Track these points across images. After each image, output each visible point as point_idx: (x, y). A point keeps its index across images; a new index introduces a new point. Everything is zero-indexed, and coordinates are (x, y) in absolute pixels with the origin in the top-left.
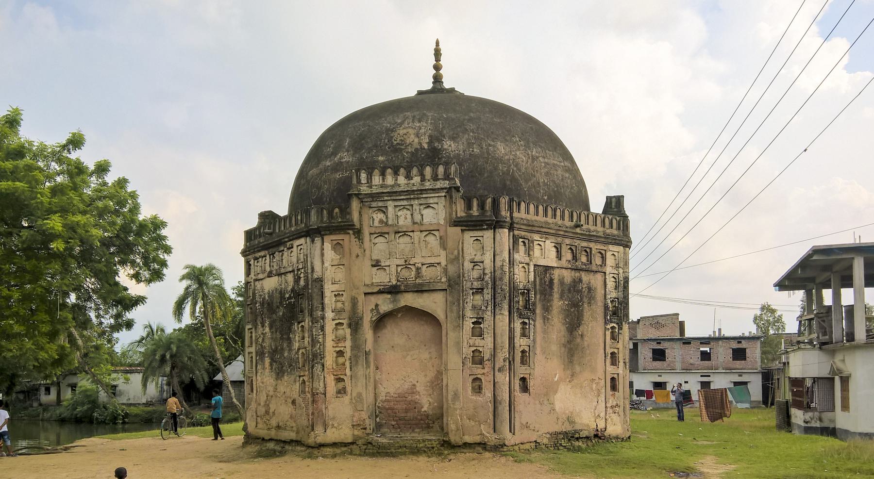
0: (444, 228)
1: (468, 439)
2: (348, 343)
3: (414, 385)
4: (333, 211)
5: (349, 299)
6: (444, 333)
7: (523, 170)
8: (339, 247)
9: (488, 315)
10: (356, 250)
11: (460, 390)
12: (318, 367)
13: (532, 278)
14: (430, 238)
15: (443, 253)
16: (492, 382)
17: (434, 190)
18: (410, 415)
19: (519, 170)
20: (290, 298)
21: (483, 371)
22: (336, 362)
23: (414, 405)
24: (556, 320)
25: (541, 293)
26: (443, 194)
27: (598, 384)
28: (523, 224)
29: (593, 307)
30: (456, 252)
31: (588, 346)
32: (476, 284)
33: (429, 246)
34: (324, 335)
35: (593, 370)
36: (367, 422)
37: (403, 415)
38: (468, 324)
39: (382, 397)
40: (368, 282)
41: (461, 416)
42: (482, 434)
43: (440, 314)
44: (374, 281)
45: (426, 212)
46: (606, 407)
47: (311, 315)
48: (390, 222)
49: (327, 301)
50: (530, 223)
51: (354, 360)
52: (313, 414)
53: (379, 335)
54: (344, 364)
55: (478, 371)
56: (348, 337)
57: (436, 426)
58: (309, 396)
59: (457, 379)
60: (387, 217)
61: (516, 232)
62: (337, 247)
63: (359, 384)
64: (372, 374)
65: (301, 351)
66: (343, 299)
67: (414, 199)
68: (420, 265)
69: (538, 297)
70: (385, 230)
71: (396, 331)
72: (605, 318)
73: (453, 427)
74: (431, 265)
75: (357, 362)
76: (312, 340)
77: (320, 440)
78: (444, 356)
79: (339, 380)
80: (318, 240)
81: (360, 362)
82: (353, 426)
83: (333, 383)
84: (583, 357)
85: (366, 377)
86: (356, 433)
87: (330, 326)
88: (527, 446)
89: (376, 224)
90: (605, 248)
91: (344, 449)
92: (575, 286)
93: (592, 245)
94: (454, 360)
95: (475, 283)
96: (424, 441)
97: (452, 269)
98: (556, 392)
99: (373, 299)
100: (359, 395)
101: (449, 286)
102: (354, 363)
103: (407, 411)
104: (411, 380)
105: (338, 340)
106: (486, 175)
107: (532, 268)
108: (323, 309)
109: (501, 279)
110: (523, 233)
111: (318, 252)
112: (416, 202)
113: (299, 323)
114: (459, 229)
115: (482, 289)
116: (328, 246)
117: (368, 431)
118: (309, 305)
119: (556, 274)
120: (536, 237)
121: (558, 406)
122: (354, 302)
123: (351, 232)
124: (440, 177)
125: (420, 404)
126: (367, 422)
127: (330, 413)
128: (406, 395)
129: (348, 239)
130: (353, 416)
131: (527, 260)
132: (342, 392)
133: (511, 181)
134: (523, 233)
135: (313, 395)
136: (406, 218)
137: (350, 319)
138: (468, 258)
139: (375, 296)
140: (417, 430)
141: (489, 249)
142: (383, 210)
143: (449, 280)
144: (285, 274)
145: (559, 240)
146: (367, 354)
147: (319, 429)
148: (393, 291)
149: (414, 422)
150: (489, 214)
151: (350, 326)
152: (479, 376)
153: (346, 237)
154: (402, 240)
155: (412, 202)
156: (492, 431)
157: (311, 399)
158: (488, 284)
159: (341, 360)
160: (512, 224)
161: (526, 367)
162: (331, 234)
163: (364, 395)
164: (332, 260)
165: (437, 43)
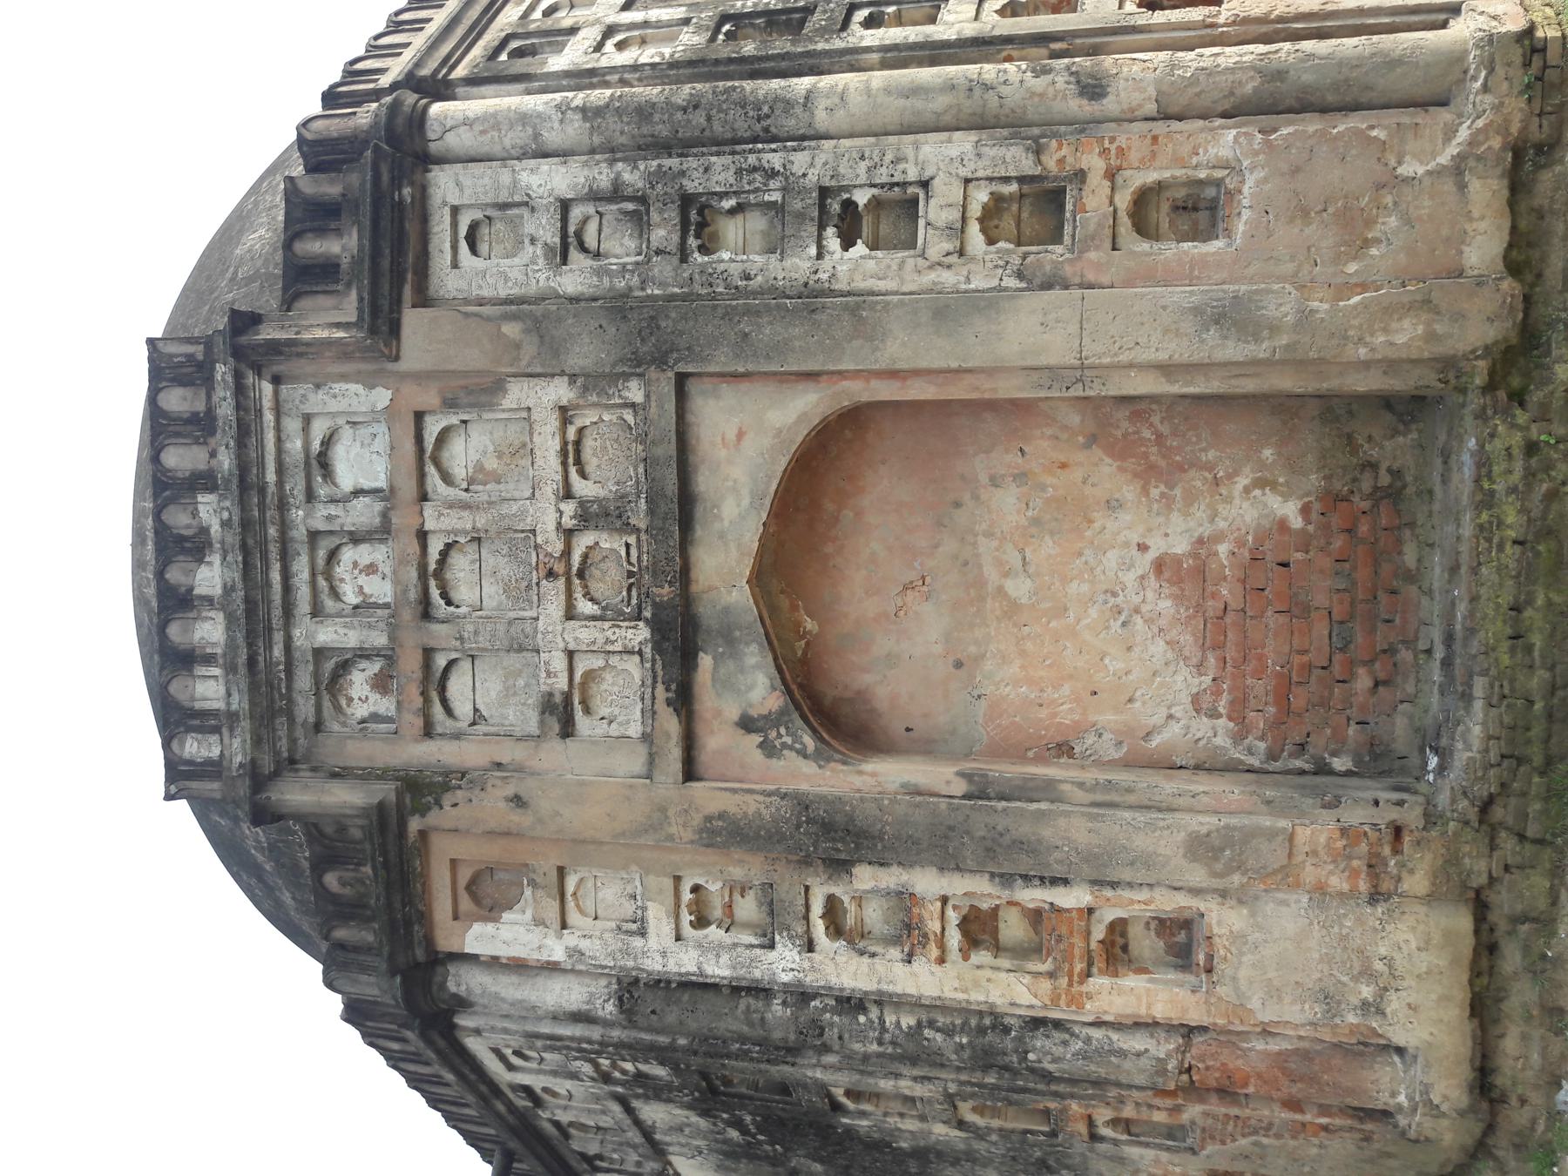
0: (409, 389)
1: (1483, 247)
2: (927, 883)
3: (1159, 566)
4: (334, 898)
5: (712, 856)
6: (885, 391)
8: (487, 888)
9: (810, 166)
10: (491, 805)
11: (1180, 295)
12: (1043, 1049)
14: (461, 456)
15: (517, 394)
16: (1160, 127)
17: (245, 431)
18: (1321, 592)
20: (738, 1124)
21: (1096, 180)
22: (1023, 952)
23: (1268, 561)
26: (267, 388)
30: (511, 330)
32: (663, 233)
33: (492, 464)
34: (882, 1000)
36: (1356, 816)
37: (1321, 629)
38: (852, 265)
39: (1217, 733)
40: (637, 763)
41: (1345, 289)
42: (1458, 169)
43: (794, 412)
44: (635, 730)
45: (346, 477)
47: (791, 1051)
48: (380, 640)
49: (719, 969)
51: (1014, 860)
52: (1293, 1105)
53: (897, 727)
54: (1036, 917)
55: (1095, 203)
56: (891, 878)
57: (1393, 449)
58: (1193, 1112)
59: (1133, 317)
60: (363, 654)
62: (486, 895)
63: (1141, 842)
64: (1090, 776)
65: (971, 1117)
66: (714, 887)
67: (284, 526)
68: (569, 508)
70: (410, 663)
71: (884, 644)
73: (1406, 334)
74: (572, 455)
75: (1019, 845)
76: (914, 1061)
77: (1450, 1089)
78: (1008, 388)
79: (1116, 951)
80: (463, 981)
81: (1024, 830)
82: (1375, 897)
83: (1131, 981)
85: (1105, 803)
86: (1417, 882)
87: (841, 969)
89: (385, 705)
91: (1511, 959)
94: (1035, 334)
96: (1487, 501)
97: (586, 352)
99: (718, 739)
100: (1202, 848)
101: (660, 361)
102: (1025, 864)
103: (1296, 609)
104: (1130, 578)
105: (908, 933)
108: (761, 991)
109: (644, 112)
111: (509, 988)
112: (297, 515)
113: (836, 1107)
114: (412, 319)
115: (687, 201)
116: (479, 938)
117: (1412, 816)
118: (743, 1055)
122: (725, 834)
123: (414, 824)
124: (200, 406)
125: (1260, 539)
126: (1356, 816)
127: (1295, 1014)
128: (1213, 607)
129: (453, 840)
130: (1320, 889)
132: (1182, 943)
135: (1193, 1091)
136: (371, 569)
137: (806, 862)
138: (542, 278)
139: (700, 729)
140: (1410, 557)
141: (505, 177)
142: (334, 670)
143: (635, 365)
144: (647, 1133)
146: (980, 790)
147: (1389, 1086)
148: (678, 639)
149: (1363, 574)
150: (354, 179)
151: (839, 867)
152: (1123, 200)
153: (443, 850)
154: (464, 593)
155: (299, 533)
156: (1444, 115)
157: (1219, 1108)
158: (660, 174)
159: (1013, 928)
162: (425, 918)
163: (1205, 823)
164: (539, 922)
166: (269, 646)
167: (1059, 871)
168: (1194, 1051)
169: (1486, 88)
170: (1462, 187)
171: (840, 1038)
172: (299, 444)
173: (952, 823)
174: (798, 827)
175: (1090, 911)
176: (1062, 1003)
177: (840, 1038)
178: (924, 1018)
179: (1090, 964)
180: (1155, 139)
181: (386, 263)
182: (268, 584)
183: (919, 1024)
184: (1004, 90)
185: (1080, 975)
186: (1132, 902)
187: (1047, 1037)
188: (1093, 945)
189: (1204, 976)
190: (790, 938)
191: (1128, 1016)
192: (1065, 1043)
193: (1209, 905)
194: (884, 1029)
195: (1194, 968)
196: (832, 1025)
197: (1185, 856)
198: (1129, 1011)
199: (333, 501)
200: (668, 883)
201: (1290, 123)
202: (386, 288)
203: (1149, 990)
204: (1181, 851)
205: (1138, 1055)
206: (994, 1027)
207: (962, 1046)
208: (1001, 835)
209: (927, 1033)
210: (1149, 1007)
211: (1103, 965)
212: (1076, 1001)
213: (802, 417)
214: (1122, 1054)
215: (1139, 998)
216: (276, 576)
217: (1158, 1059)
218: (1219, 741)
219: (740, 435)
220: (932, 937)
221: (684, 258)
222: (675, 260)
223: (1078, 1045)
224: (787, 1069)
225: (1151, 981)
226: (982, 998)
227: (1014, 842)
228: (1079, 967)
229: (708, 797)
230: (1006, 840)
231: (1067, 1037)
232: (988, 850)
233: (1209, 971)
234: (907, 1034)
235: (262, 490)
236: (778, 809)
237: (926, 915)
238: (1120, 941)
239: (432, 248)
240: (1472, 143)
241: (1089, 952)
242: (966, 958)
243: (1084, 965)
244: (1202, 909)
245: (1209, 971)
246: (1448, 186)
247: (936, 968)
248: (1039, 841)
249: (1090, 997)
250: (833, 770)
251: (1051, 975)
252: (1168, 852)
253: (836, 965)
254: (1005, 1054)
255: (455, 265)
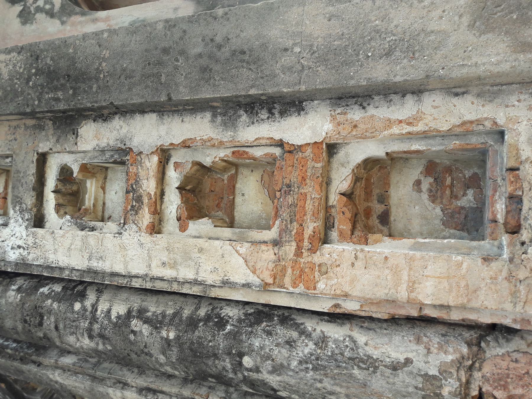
79: (368, 209)
102: (246, 85)
167: (284, 85)
168: (487, 369)
171: (57, 328)
173: (165, 44)
174: (28, 80)
175: (332, 149)
176: (287, 281)
177: (57, 328)
178: (136, 306)
179: (328, 225)
183: (129, 314)
185: (311, 239)
186: (389, 123)
187: (269, 333)
188: (334, 199)
189: (505, 239)
190: (22, 211)
191: (379, 303)
192: (290, 343)
193: (512, 112)
194: (94, 319)
195: (488, 229)
196: (50, 312)
197: (471, 26)
198: (381, 293)
203: (412, 259)
204: (466, 20)
205: (395, 367)
206: (208, 318)
207: (167, 341)
208: (219, 47)
209: (136, 324)
210: (411, 289)
211: (346, 227)
212: (305, 277)
214: (371, 364)
215: (396, 271)
217: (427, 377)
220: (146, 200)
223: (307, 348)
224: (33, 368)
225: (415, 247)
226: (190, 275)
227: (234, 53)
228: (311, 227)
230: (226, 52)
231: (295, 334)
232: (204, 70)
233: (514, 230)
234: (115, 325)
236: (15, 66)
237: (142, 173)
238: (379, 208)
241: (328, 208)
242: (183, 228)
243: (319, 224)
244: (501, 121)
245: (514, 230)
247: (146, 238)
248: (264, 46)
249: (323, 270)
250: (73, 24)
251: (276, 243)
252: (444, 25)
253: (54, 239)
254: (216, 356)
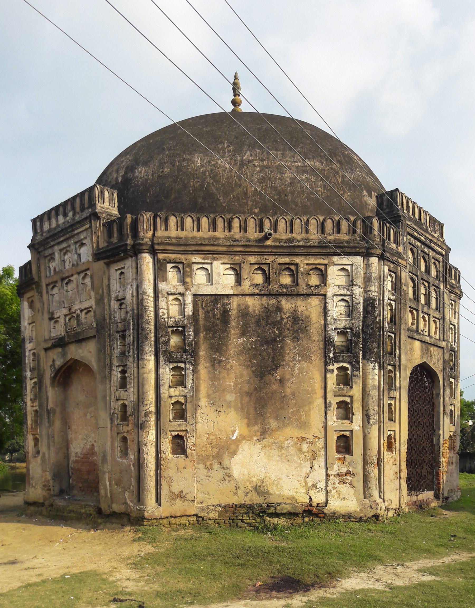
7: (223, 180)
13: (189, 310)
16: (136, 442)
19: (218, 182)
24: (234, 363)
25: (208, 329)
27: (311, 443)
28: (168, 244)
29: (304, 342)
31: (293, 394)
35: (303, 425)
42: (126, 503)
46: (327, 475)
50: (183, 242)
61: (161, 256)
69: (202, 335)
72: (326, 354)
84: (282, 408)
88: (183, 520)
90: (326, 262)
92: (268, 317)
93: (297, 260)
95: (120, 325)
98: (234, 453)
104: (90, 439)
106: (173, 197)
107: (189, 299)
110: (173, 256)
119: (234, 303)
120: (196, 259)
121: (237, 471)
131: (181, 289)
133: (204, 198)
134: (173, 256)
145: (237, 258)
160: (152, 246)
161: (182, 422)
165: (236, 78)
166: (52, 241)
169: (137, 509)
170: (123, 504)
172: (82, 237)
180: (133, 441)
181: (108, 254)
182: (60, 237)
184: (142, 406)
199: (76, 249)
200: (34, 347)
201: (135, 469)
202: (104, 255)
213: (93, 366)
216: (62, 239)
218: (72, 458)
219: (90, 352)
221: (118, 332)
222: (116, 330)
229: (42, 354)
235: (73, 230)
239: (118, 263)
240: (130, 506)
246: (123, 501)
255: (116, 270)
